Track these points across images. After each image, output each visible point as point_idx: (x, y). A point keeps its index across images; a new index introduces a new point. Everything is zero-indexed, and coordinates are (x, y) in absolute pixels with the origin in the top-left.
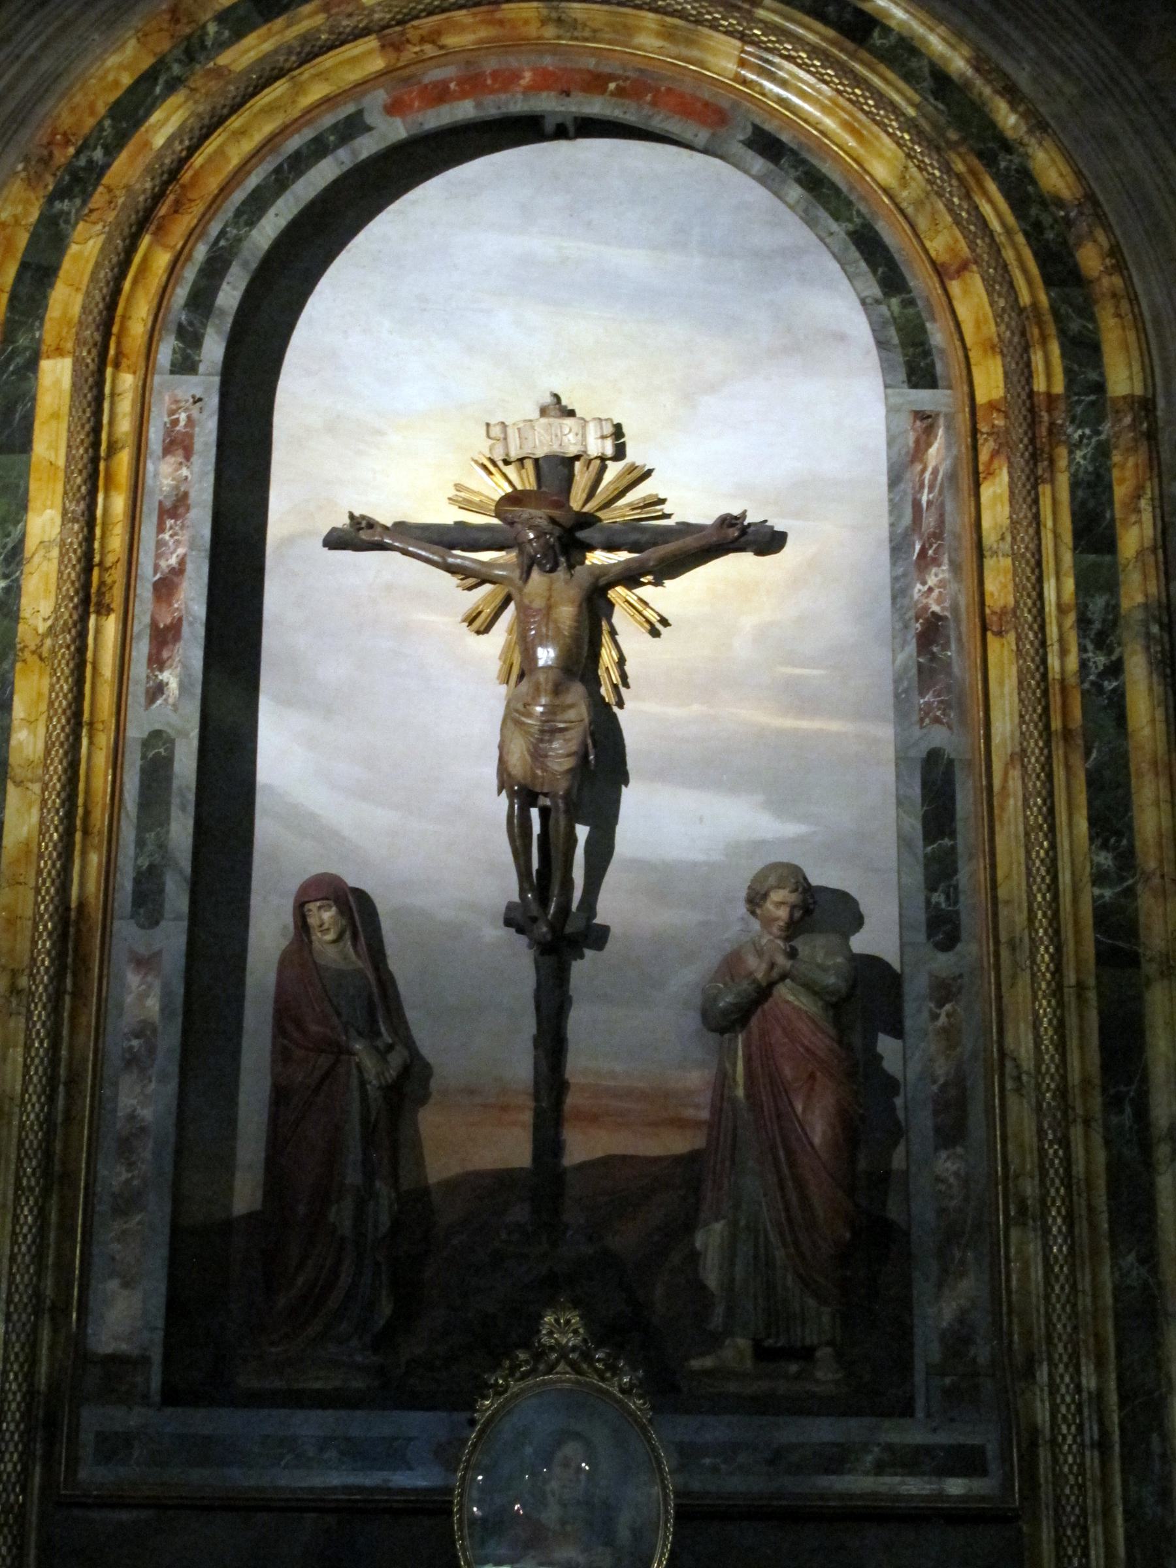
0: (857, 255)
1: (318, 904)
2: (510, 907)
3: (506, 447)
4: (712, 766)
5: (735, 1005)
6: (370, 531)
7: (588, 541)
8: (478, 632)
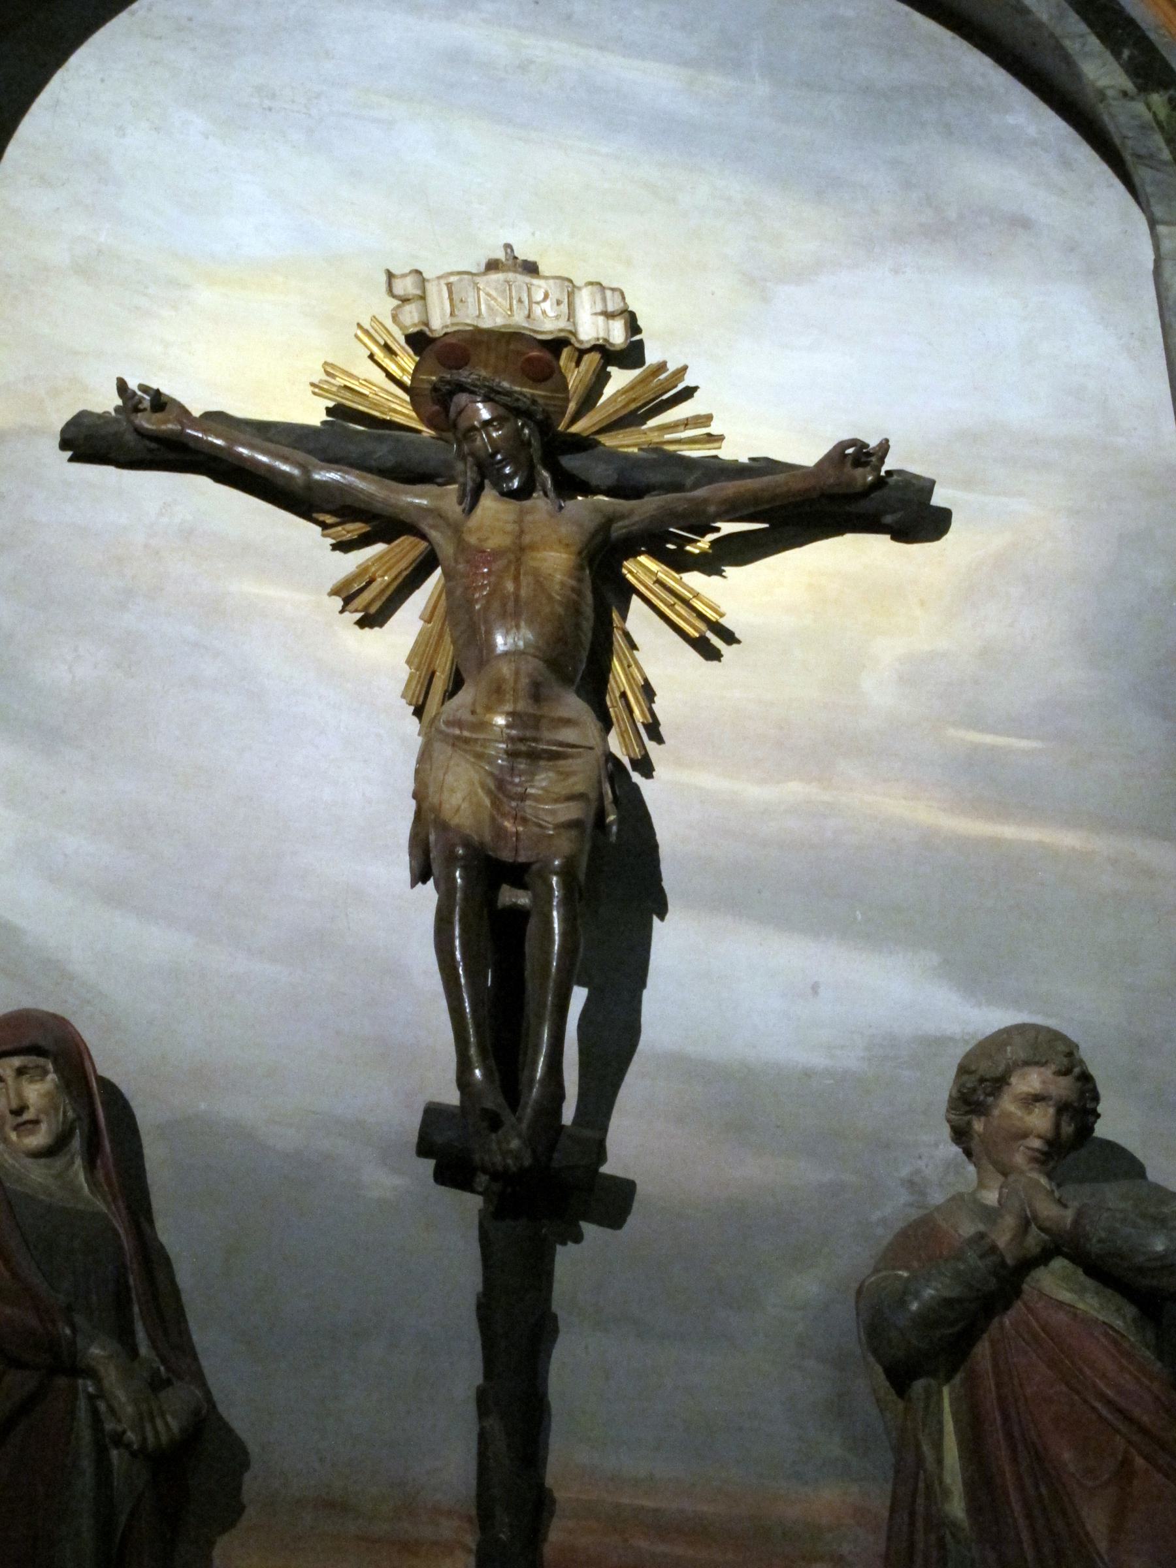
0: (1083, 27)
1: (17, 1061)
2: (433, 1114)
3: (425, 309)
4: (831, 892)
5: (948, 1302)
6: (159, 415)
7: (583, 476)
8: (362, 623)
